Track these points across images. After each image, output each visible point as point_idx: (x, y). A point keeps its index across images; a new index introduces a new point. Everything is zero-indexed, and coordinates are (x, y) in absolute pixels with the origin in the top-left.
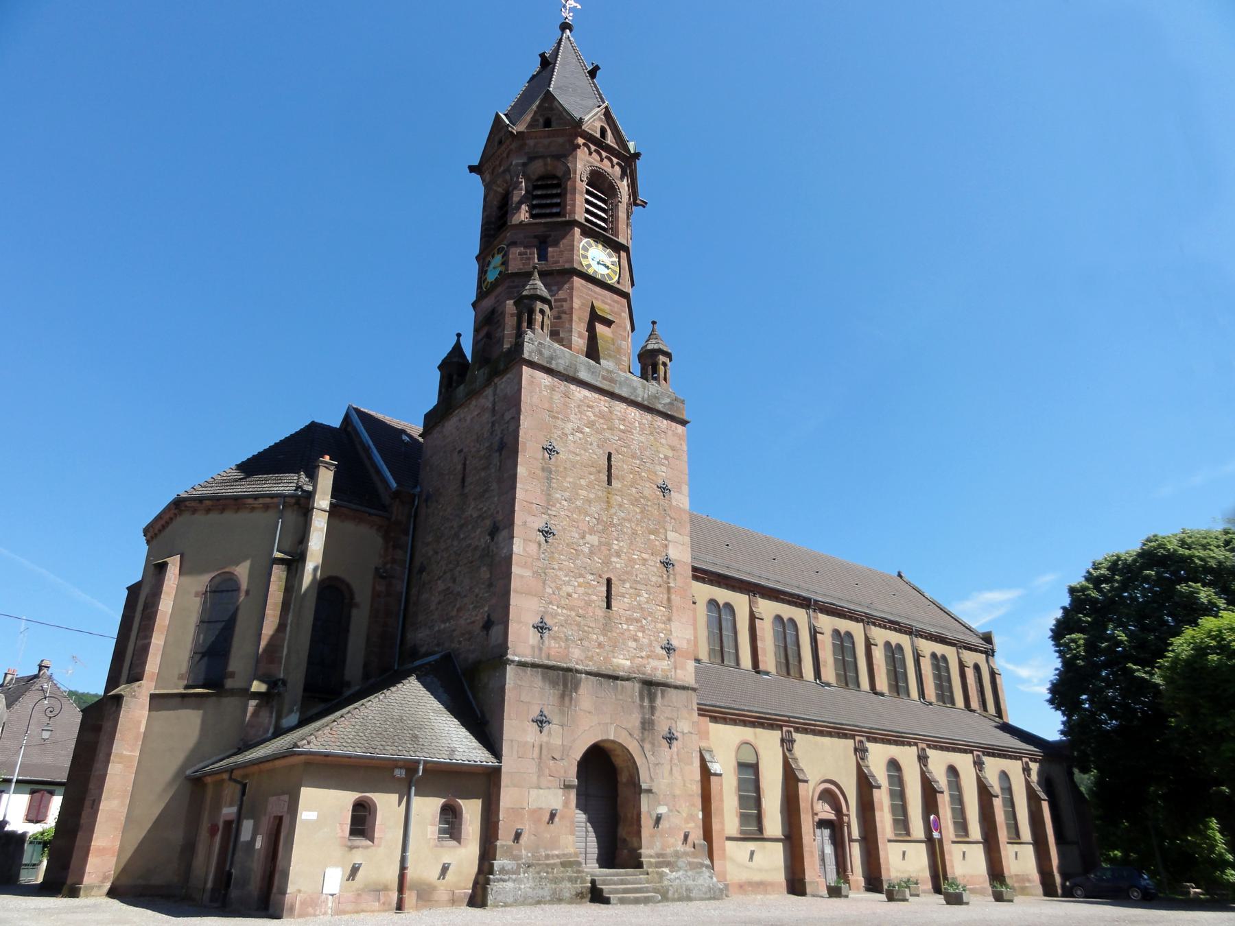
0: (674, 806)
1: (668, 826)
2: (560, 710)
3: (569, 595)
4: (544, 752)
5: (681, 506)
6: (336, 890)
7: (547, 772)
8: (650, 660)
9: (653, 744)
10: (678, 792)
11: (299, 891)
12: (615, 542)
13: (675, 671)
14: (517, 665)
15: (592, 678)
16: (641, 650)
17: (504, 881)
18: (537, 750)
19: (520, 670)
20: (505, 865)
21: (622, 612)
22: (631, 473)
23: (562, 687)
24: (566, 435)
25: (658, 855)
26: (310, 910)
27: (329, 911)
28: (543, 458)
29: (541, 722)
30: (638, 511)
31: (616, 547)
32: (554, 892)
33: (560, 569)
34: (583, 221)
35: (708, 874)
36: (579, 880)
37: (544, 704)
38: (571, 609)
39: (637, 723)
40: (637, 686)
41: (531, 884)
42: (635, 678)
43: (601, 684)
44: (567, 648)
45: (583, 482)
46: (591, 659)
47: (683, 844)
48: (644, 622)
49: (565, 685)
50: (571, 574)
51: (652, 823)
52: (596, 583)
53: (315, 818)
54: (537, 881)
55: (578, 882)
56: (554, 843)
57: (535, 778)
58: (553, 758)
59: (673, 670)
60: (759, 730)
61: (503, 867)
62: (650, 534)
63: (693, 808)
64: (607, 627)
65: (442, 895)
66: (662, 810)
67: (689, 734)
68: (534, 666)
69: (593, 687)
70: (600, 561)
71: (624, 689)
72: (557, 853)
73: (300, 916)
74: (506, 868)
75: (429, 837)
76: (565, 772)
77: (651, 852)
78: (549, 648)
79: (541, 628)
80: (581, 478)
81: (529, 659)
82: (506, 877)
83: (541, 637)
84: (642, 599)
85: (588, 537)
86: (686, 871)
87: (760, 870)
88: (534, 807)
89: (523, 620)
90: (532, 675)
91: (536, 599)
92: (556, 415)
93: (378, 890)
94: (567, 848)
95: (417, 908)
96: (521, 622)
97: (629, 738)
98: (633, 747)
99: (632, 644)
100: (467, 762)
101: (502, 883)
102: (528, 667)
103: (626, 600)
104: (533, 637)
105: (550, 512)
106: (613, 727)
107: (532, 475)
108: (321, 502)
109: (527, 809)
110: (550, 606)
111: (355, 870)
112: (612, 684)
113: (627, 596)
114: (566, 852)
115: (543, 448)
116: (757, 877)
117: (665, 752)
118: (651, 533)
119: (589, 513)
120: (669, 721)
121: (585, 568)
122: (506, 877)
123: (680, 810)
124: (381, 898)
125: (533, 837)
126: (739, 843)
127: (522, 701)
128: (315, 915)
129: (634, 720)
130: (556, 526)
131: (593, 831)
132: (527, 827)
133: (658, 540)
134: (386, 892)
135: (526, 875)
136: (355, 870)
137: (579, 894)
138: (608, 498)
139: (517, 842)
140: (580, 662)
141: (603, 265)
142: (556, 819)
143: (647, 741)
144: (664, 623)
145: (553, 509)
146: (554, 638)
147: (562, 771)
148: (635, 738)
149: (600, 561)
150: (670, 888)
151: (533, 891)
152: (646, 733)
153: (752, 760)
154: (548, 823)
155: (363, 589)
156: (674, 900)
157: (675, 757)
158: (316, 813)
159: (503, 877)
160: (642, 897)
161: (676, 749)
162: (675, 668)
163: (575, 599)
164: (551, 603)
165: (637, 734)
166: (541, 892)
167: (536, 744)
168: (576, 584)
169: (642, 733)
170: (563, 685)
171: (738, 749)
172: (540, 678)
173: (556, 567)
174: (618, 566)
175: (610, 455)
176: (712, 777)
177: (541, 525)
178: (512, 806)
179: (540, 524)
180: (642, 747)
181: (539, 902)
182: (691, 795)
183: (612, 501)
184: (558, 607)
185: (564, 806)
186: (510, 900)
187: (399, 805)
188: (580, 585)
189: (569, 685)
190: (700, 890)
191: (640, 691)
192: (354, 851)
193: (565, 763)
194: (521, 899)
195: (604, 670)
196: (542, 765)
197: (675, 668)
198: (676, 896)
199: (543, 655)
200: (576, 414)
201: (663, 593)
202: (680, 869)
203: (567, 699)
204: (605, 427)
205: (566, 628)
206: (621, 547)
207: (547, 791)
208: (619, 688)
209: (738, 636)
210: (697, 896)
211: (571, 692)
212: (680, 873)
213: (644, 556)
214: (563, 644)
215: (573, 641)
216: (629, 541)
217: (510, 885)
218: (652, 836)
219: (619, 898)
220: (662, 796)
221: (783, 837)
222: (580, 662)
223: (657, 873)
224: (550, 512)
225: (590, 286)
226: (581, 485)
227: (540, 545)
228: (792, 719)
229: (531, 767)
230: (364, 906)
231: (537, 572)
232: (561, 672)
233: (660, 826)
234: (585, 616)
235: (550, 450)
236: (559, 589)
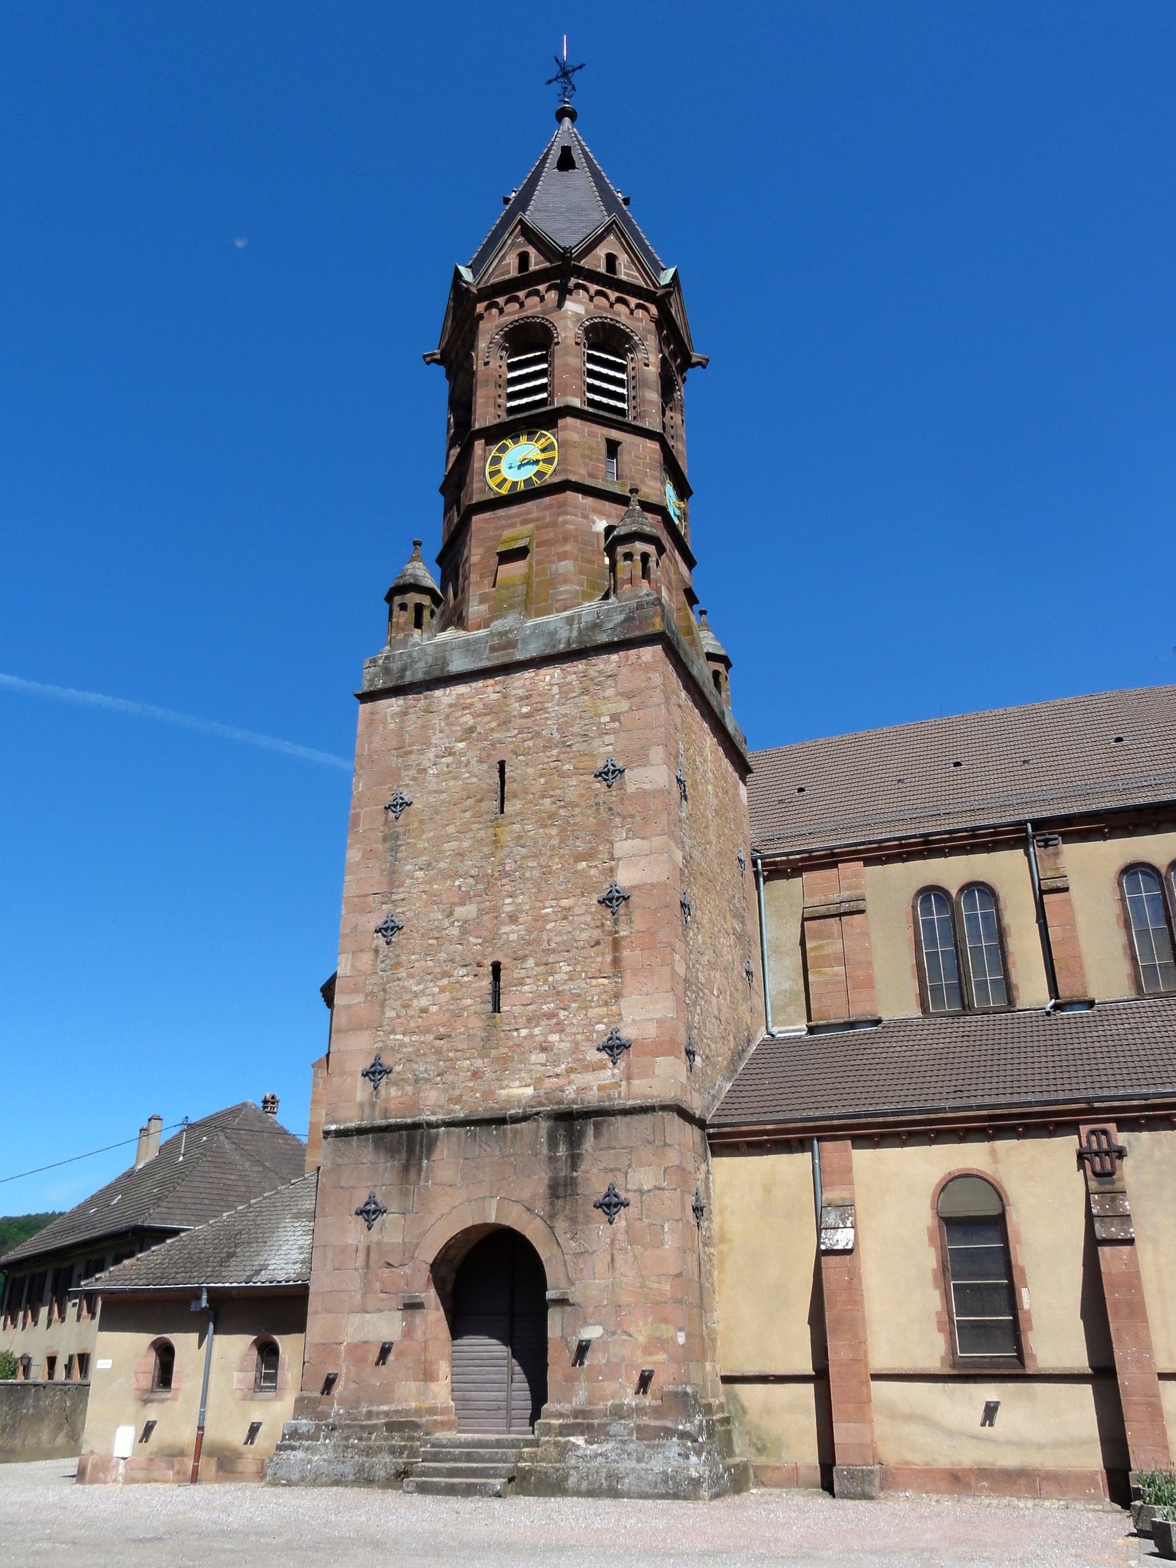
0: (619, 1324)
1: (604, 1361)
2: (401, 1190)
3: (424, 1010)
4: (373, 1256)
5: (647, 787)
6: (127, 1453)
8: (573, 1076)
9: (573, 1220)
10: (625, 1299)
11: (92, 1452)
12: (508, 900)
13: (629, 1084)
14: (336, 1137)
15: (457, 1130)
16: (556, 1063)
17: (293, 1448)
18: (361, 1256)
20: (299, 1426)
21: (517, 1010)
22: (542, 776)
23: (404, 1155)
25: (577, 1413)
26: (101, 1475)
27: (120, 1478)
28: (386, 823)
29: (370, 1213)
30: (554, 833)
31: (507, 909)
32: (361, 1469)
33: (411, 976)
34: (505, 418)
35: (677, 1449)
36: (406, 1453)
37: (375, 1186)
38: (427, 1031)
39: (542, 1189)
41: (330, 1454)
42: (537, 1114)
43: (474, 1136)
44: (417, 1093)
45: (451, 829)
46: (458, 1100)
47: (637, 1393)
49: (411, 1150)
50: (429, 977)
51: (569, 1355)
53: (109, 1367)
54: (340, 1450)
55: (405, 1456)
56: (386, 1394)
57: (358, 1298)
58: (388, 1264)
59: (624, 1083)
60: (1001, 1145)
61: (296, 1430)
62: (576, 862)
63: (662, 1326)
64: (489, 1040)
65: (248, 1464)
66: (592, 1333)
67: (657, 1192)
68: (360, 1131)
69: (459, 1143)
70: (480, 941)
72: (385, 1408)
73: (92, 1482)
74: (300, 1431)
76: (407, 1284)
78: (387, 1100)
79: (376, 1072)
80: (447, 825)
81: (352, 1125)
82: (297, 1444)
83: (375, 1088)
86: (623, 1442)
87: (1020, 1444)
89: (347, 1069)
90: (358, 1146)
91: (367, 1033)
92: (409, 749)
93: (172, 1454)
94: (406, 1401)
95: (217, 1480)
97: (527, 1216)
98: (533, 1230)
99: (538, 1057)
100: (267, 1284)
101: (289, 1452)
102: (352, 1135)
105: (394, 897)
106: (494, 1202)
107: (368, 854)
110: (392, 1037)
111: (149, 1428)
112: (495, 1132)
113: (528, 981)
114: (404, 1406)
116: (1009, 1460)
117: (600, 1230)
118: (579, 858)
119: (461, 871)
120: (610, 1174)
121: (451, 960)
122: (297, 1444)
123: (632, 1330)
124: (175, 1465)
125: (353, 1386)
126: (951, 1386)
127: (342, 1188)
128: (105, 1482)
129: (537, 1183)
131: (522, 1372)
132: (344, 1370)
133: (596, 866)
135: (327, 1441)
136: (149, 1428)
137: (402, 1473)
138: (495, 835)
139: (328, 1394)
140: (438, 1109)
141: (528, 463)
142: (391, 1357)
143: (561, 1217)
144: (606, 1004)
145: (400, 890)
146: (396, 1084)
147: (402, 1284)
148: (538, 1215)
149: (480, 941)
150: (572, 1472)
151: (329, 1465)
152: (560, 1202)
153: (992, 1210)
154: (377, 1364)
156: (578, 1493)
157: (621, 1236)
158: (110, 1361)
159: (294, 1443)
160: (461, 1483)
163: (433, 1014)
164: (393, 1032)
165: (541, 1207)
166: (340, 1468)
167: (361, 1247)
169: (552, 1204)
170: (407, 1152)
171: (995, 1189)
172: (371, 1148)
173: (404, 975)
175: (502, 764)
178: (323, 1342)
179: (377, 920)
181: (336, 1483)
182: (656, 1303)
183: (502, 838)
184: (403, 1034)
185: (404, 1337)
186: (295, 1477)
187: (200, 1347)
188: (442, 990)
189: (418, 1148)
190: (639, 1478)
191: (548, 1134)
192: (149, 1405)
193: (407, 1270)
194: (311, 1477)
195: (481, 1112)
196: (369, 1276)
198: (584, 1486)
199: (377, 1112)
200: (441, 731)
201: (603, 954)
202: (609, 1436)
203: (413, 1171)
205: (417, 1063)
206: (519, 904)
207: (375, 1316)
208: (509, 1135)
210: (633, 1488)
212: (609, 1446)
213: (565, 903)
214: (409, 1089)
215: (426, 1080)
216: (535, 890)
217: (300, 1454)
218: (570, 1379)
219: (417, 1483)
220: (591, 1309)
221: (1090, 1371)
222: (438, 1109)
223: (556, 1444)
224: (394, 897)
225: (500, 512)
226: (448, 836)
227: (376, 951)
228: (1096, 1105)
229: (353, 1282)
230: (156, 1474)
231: (372, 993)
232: (404, 1133)
233: (586, 1363)
234: (450, 1036)
235: (398, 806)
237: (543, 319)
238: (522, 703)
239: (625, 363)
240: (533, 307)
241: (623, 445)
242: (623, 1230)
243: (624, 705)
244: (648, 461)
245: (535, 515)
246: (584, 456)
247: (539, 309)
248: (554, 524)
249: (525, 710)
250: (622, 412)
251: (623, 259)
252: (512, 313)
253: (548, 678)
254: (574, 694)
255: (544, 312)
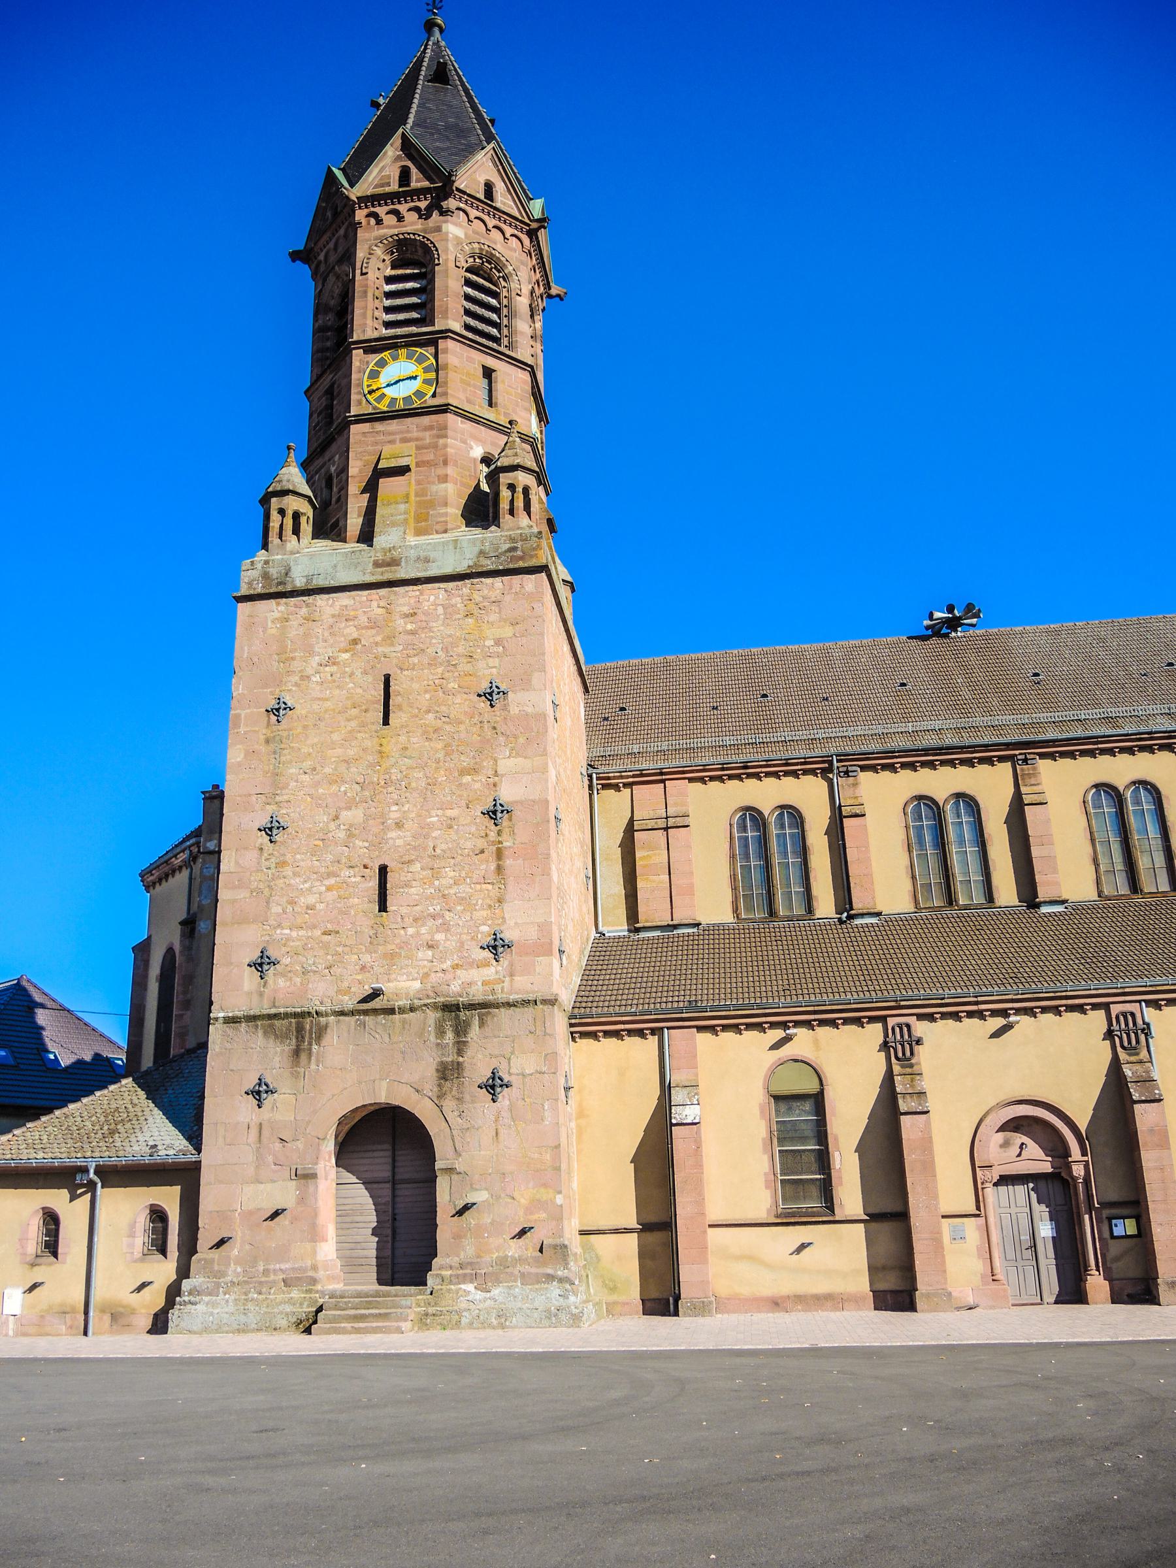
3: (311, 907)
7: (270, 1159)
12: (394, 808)
18: (254, 1132)
19: (229, 1030)
24: (308, 677)
29: (259, 1092)
33: (295, 874)
40: (432, 1016)
41: (231, 1308)
48: (448, 915)
52: (358, 879)
55: (305, 1306)
71: (407, 1026)
75: (125, 1251)
77: (454, 1261)
79: (262, 964)
82: (198, 1299)
84: (444, 881)
85: (345, 815)
88: (250, 1208)
96: (232, 964)
101: (190, 1306)
103: (413, 890)
104: (250, 978)
105: (278, 799)
108: (208, 844)
109: (239, 1210)
115: (267, 711)
123: (516, 1195)
125: (247, 1247)
130: (285, 815)
134: (73, 1315)
143: (449, 1097)
146: (283, 975)
149: (366, 844)
155: (177, 948)
161: (508, 1103)
162: (512, 975)
165: (430, 1087)
168: (323, 888)
174: (399, 842)
176: (1136, 1106)
177: (264, 821)
180: (440, 1107)
188: (329, 889)
192: (36, 1268)
197: (512, 975)
204: (379, 639)
206: (404, 812)
208: (398, 1024)
209: (988, 848)
211: (310, 1044)
225: (379, 426)
236: (292, 902)
237: (424, 237)
238: (407, 619)
239: (498, 290)
240: (413, 224)
241: (498, 373)
242: (506, 1108)
243: (508, 632)
244: (519, 391)
245: (415, 434)
246: (462, 381)
247: (420, 226)
248: (435, 446)
249: (409, 627)
250: (496, 340)
251: (500, 188)
252: (390, 227)
253: (432, 598)
254: (458, 616)
255: (425, 231)
